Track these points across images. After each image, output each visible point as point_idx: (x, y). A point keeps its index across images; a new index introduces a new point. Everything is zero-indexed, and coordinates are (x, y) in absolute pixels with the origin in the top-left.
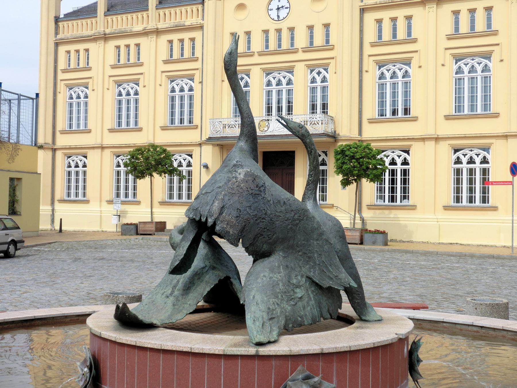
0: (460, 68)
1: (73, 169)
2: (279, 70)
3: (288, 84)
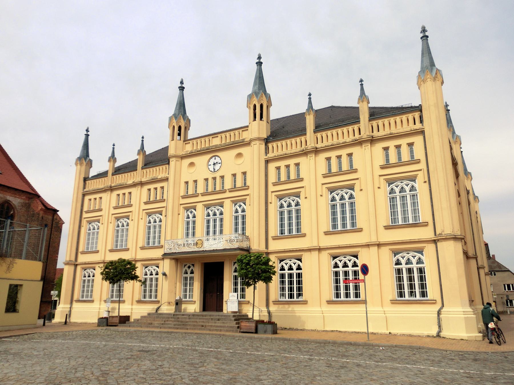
0: (392, 189)
1: (341, 269)
2: (215, 205)
3: (296, 205)
